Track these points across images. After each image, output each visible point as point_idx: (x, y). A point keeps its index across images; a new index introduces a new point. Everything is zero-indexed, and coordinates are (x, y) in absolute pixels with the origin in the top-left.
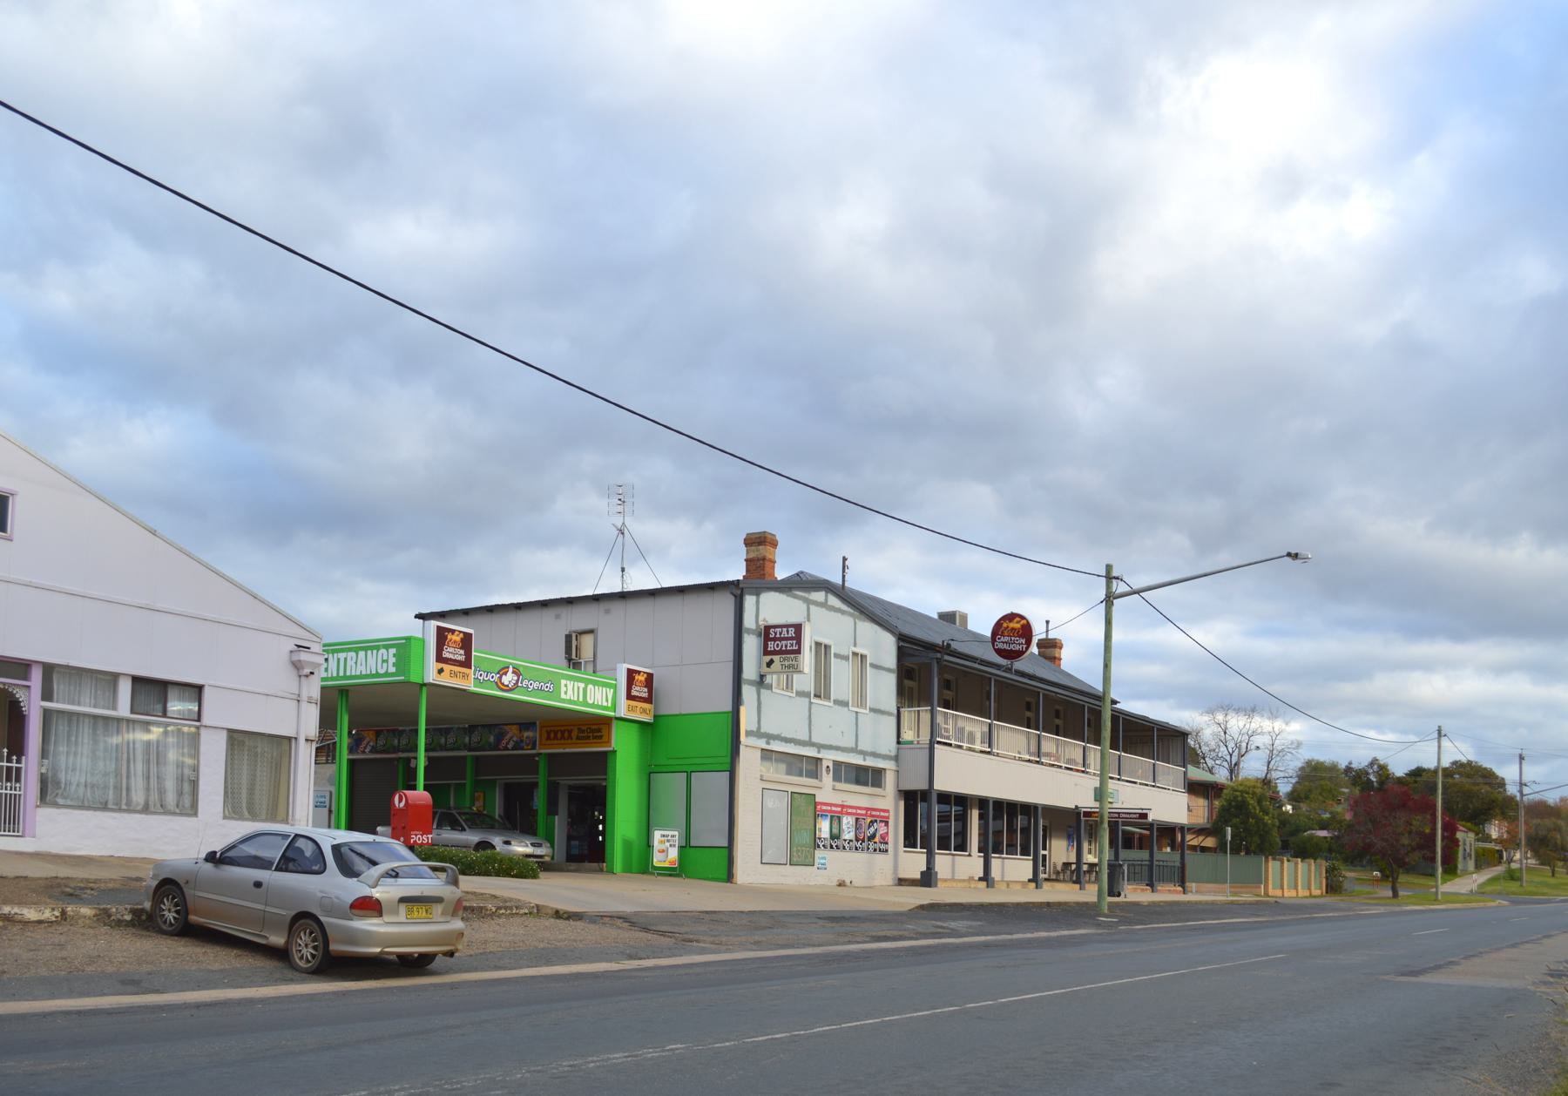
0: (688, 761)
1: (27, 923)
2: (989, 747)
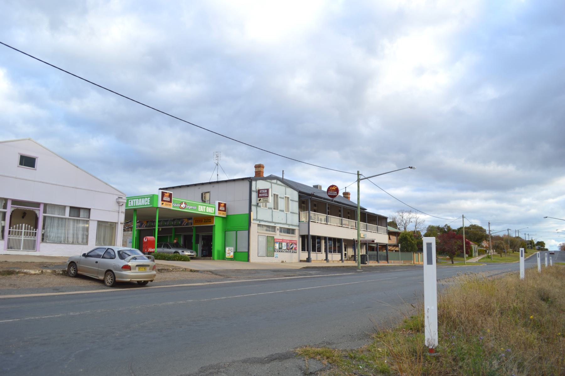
0: (236, 228)
1: (31, 274)
2: (327, 222)
